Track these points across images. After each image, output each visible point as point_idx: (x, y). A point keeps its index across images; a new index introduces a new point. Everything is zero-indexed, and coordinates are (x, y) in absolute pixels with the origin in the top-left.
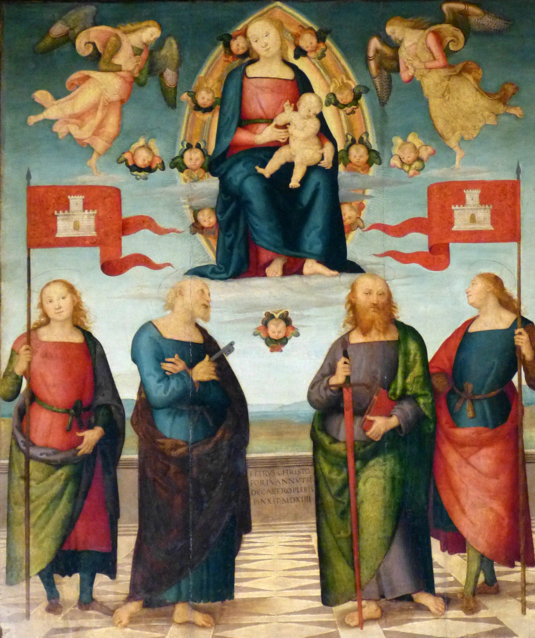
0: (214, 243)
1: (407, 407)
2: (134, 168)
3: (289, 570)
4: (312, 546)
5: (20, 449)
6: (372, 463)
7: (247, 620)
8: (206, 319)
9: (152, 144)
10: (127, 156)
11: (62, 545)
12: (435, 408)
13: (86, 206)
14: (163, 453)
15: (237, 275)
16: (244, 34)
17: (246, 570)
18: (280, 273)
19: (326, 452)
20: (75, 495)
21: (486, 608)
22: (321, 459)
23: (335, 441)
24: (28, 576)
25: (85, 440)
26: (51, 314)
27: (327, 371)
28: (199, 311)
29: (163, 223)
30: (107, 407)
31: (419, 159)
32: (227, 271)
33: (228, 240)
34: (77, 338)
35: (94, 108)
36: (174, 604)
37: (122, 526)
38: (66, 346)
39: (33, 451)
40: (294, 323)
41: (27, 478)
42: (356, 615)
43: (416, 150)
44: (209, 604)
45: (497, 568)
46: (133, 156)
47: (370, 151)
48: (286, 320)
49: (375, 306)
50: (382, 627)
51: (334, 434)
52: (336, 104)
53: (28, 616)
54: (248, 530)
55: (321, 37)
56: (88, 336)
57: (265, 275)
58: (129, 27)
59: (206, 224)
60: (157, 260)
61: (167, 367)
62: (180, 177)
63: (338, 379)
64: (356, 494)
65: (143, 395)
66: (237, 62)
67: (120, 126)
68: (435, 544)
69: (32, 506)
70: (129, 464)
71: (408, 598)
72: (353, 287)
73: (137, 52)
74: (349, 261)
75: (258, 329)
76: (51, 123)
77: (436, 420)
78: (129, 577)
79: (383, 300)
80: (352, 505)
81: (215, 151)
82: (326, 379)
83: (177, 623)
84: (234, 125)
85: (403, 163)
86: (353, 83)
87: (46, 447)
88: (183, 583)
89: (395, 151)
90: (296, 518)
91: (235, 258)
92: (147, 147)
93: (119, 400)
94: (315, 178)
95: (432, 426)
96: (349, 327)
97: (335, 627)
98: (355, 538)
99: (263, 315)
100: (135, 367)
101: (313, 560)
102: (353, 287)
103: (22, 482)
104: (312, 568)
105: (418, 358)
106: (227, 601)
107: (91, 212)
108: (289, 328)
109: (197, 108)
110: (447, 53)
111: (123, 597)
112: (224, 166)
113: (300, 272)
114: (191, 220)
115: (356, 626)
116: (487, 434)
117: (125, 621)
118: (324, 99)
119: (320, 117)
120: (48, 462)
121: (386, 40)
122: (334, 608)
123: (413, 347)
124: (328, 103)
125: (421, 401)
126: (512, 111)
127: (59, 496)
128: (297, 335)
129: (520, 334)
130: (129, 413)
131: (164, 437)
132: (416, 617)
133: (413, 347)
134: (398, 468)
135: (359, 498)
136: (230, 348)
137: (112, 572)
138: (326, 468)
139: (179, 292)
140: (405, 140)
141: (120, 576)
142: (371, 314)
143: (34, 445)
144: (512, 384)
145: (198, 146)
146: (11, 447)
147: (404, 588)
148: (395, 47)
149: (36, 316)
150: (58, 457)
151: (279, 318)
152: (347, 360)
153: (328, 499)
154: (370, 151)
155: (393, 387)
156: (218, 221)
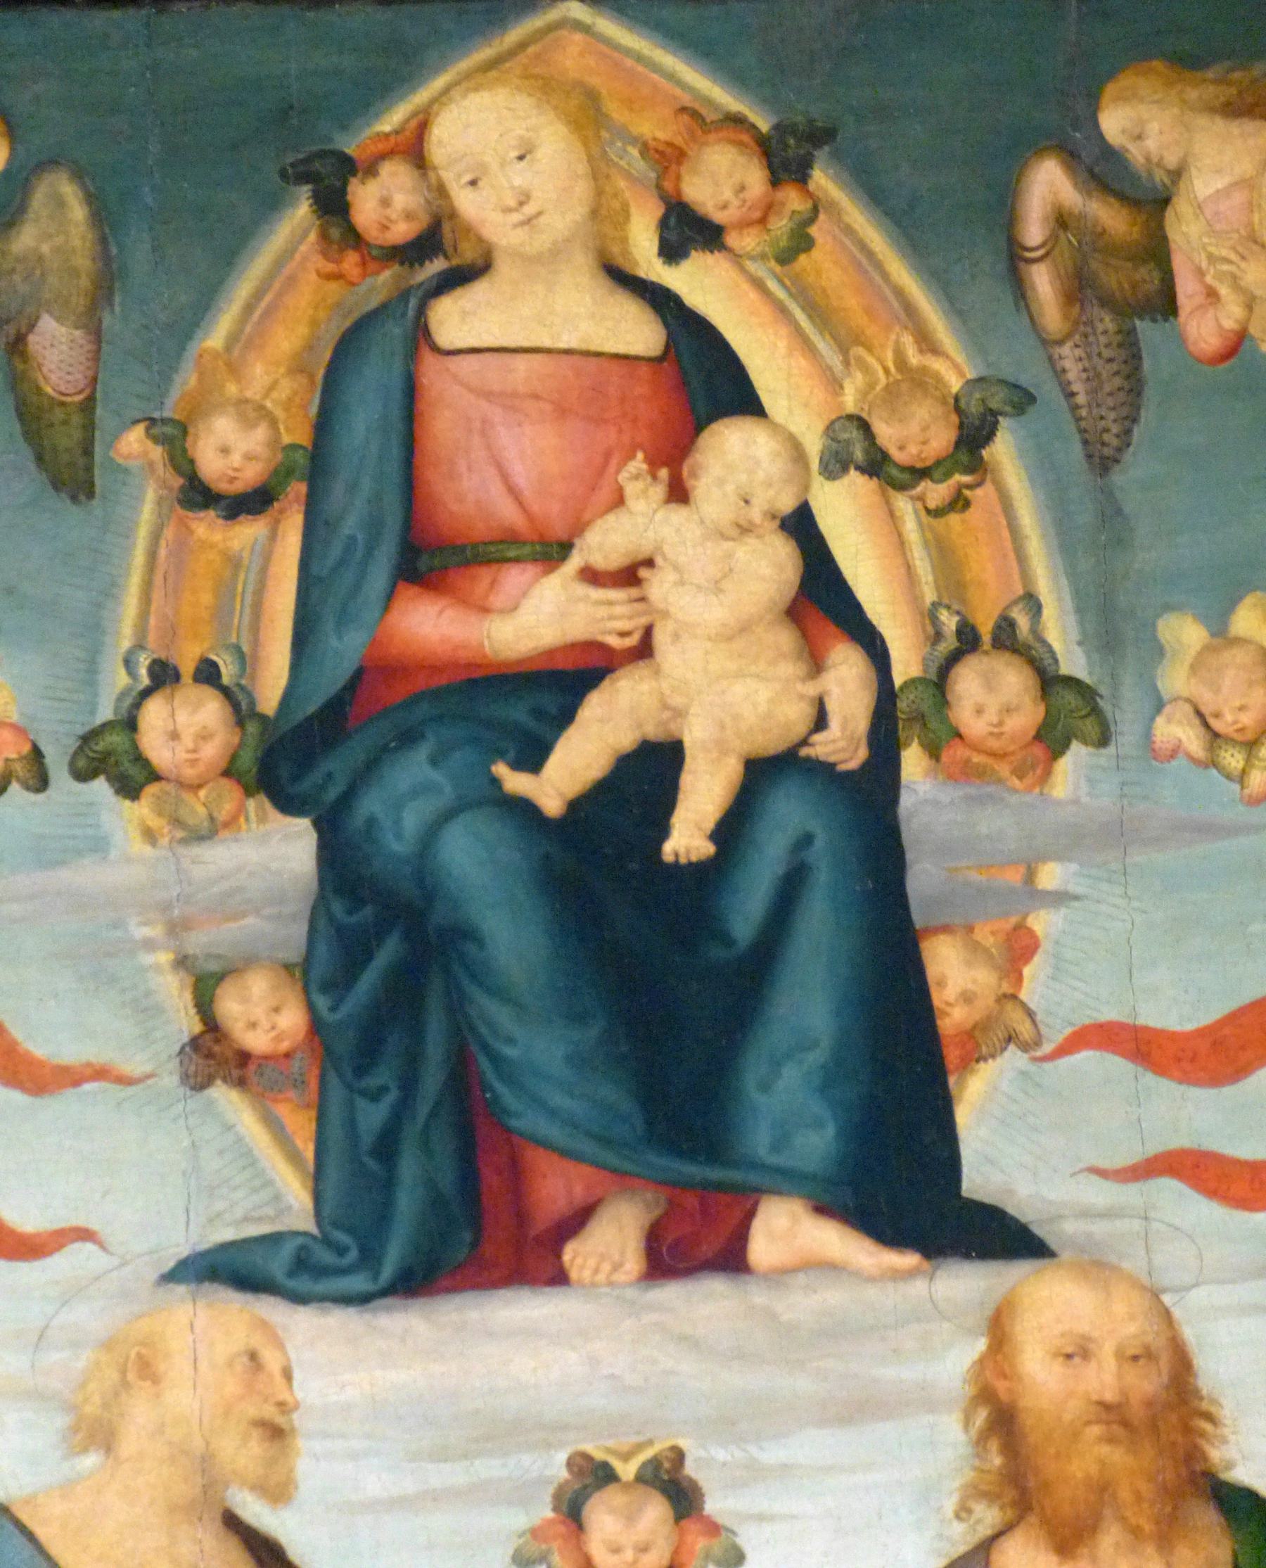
18: (634, 1263)
32: (369, 1258)
33: (373, 1116)
40: (713, 1505)
59: (257, 1042)
96: (988, 1517)
99: (556, 1468)
108: (691, 1526)
118: (814, 445)
145: (208, 674)
151: (640, 1479)
156: (316, 1026)
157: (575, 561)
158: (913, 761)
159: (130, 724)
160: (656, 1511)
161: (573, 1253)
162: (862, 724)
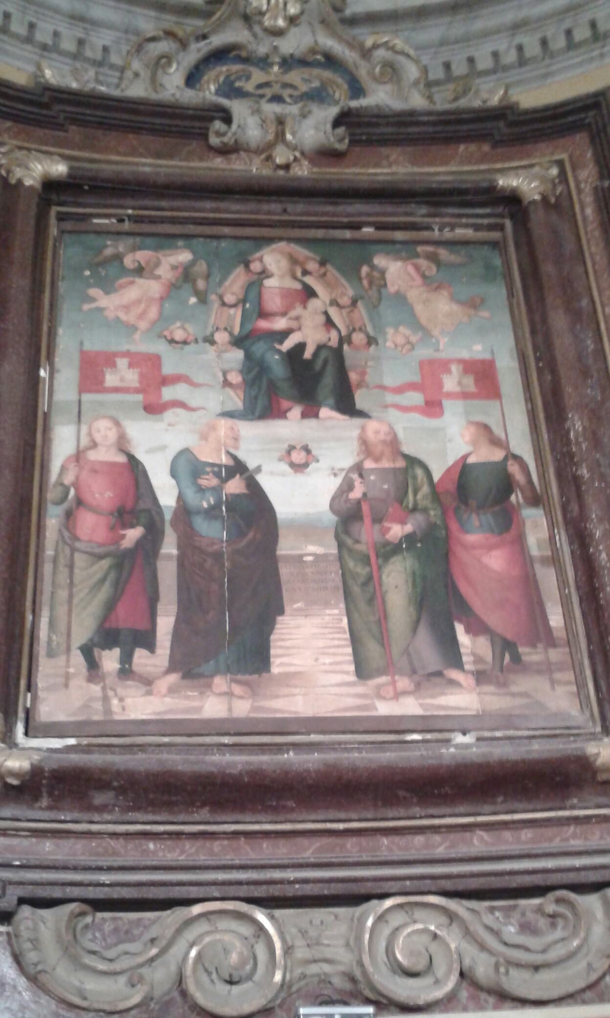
1: (419, 517)
2: (172, 341)
4: (343, 628)
5: (65, 543)
7: (286, 691)
10: (166, 333)
13: (131, 366)
16: (261, 260)
17: (281, 647)
18: (299, 416)
19: (350, 551)
20: (117, 583)
22: (346, 557)
23: (357, 542)
24: (68, 650)
25: (127, 537)
27: (346, 488)
28: (230, 442)
29: (198, 378)
30: (148, 511)
31: (409, 342)
32: (253, 413)
33: (253, 393)
34: (122, 459)
35: (138, 302)
36: (212, 676)
37: (160, 607)
39: (78, 545)
40: (314, 452)
41: (71, 567)
42: (390, 689)
43: (407, 338)
44: (247, 677)
45: (521, 650)
46: (171, 333)
48: (307, 450)
49: (384, 442)
50: (416, 699)
54: (281, 611)
55: (322, 263)
56: (132, 459)
59: (234, 382)
60: (193, 403)
61: (203, 482)
62: (211, 349)
63: (356, 494)
64: (380, 585)
65: (181, 503)
66: (256, 277)
67: (160, 314)
69: (75, 590)
70: (169, 557)
71: (439, 674)
72: (363, 429)
73: (174, 268)
74: (358, 410)
75: (282, 456)
76: (101, 310)
77: (447, 529)
78: (168, 652)
79: (389, 438)
80: (378, 594)
81: (239, 333)
82: (345, 495)
84: (255, 316)
85: (396, 346)
86: (351, 292)
89: (389, 336)
90: (327, 604)
93: (159, 506)
94: (323, 354)
95: (444, 532)
96: (362, 457)
98: (382, 620)
99: (286, 446)
102: (363, 429)
103: (66, 570)
105: (425, 479)
106: (264, 674)
108: (310, 456)
110: (424, 276)
111: (163, 669)
112: (247, 343)
113: (316, 416)
114: (221, 379)
115: (391, 699)
116: (494, 539)
118: (328, 302)
119: (326, 313)
123: (419, 472)
125: (432, 513)
127: (103, 580)
128: (318, 461)
130: (168, 516)
131: (201, 536)
133: (419, 472)
134: (417, 565)
135: (384, 588)
136: (259, 469)
137: (150, 646)
138: (351, 564)
139: (213, 428)
141: (159, 651)
145: (226, 329)
146: (57, 542)
148: (383, 272)
151: (301, 448)
152: (362, 481)
153: (356, 589)
156: (244, 380)
157: (288, 316)
158: (346, 347)
159: (213, 336)
160: (303, 454)
161: (289, 414)
162: (337, 341)
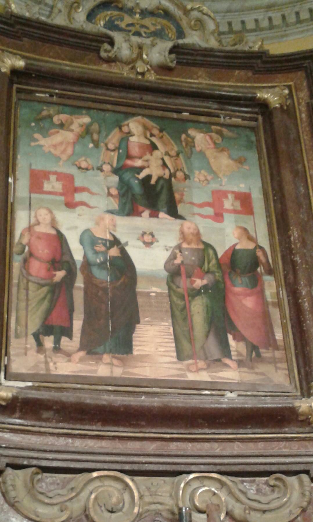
0: (117, 201)
1: (210, 276)
2: (80, 168)
3: (159, 343)
6: (197, 298)
7: (140, 364)
8: (115, 231)
9: (88, 160)
10: (77, 163)
11: (44, 323)
12: (223, 277)
13: (58, 180)
14: (96, 285)
15: (129, 215)
16: (128, 125)
18: (148, 216)
19: (174, 291)
21: (257, 368)
22: (172, 294)
23: (178, 287)
24: (26, 335)
26: (41, 220)
28: (111, 227)
29: (94, 189)
31: (206, 180)
33: (124, 201)
34: (53, 232)
35: (61, 143)
36: (102, 354)
37: (75, 315)
38: (48, 235)
39: (30, 278)
40: (156, 237)
41: (27, 289)
43: (205, 176)
47: (185, 174)
48: (152, 235)
50: (208, 372)
51: (178, 284)
52: (169, 155)
53: (26, 354)
54: (138, 322)
55: (161, 131)
56: (59, 232)
57: (141, 216)
58: (76, 116)
59: (113, 194)
60: (91, 204)
61: (97, 248)
63: (178, 261)
66: (125, 135)
67: (74, 151)
68: (230, 337)
69: (29, 303)
71: (219, 360)
73: (81, 126)
75: (139, 237)
77: (225, 283)
78: (79, 339)
79: (195, 232)
82: (172, 261)
83: (104, 363)
84: (125, 157)
85: (200, 180)
86: (176, 149)
87: (37, 277)
88: (107, 344)
89: (196, 175)
90: (162, 320)
91: (127, 208)
92: (86, 161)
94: (161, 182)
95: (223, 285)
96: (181, 241)
97: (184, 371)
99: (141, 232)
100: (81, 247)
101: (171, 339)
104: (171, 343)
107: (60, 182)
109: (108, 149)
110: (215, 143)
111: (77, 349)
113: (157, 216)
115: (195, 372)
116: (249, 291)
117: (77, 360)
118: (164, 153)
119: (163, 159)
120: (38, 284)
121: (188, 136)
122: (183, 362)
123: (211, 252)
124: (165, 155)
125: (217, 274)
126: (245, 167)
127: (44, 298)
129: (259, 251)
130: (79, 266)
132: (224, 370)
133: (211, 252)
134: (208, 301)
136: (127, 244)
137: (70, 336)
138: (175, 299)
139: (102, 219)
140: (200, 173)
141: (74, 339)
142: (191, 237)
143: (31, 275)
144: (258, 272)
145: (109, 163)
147: (217, 356)
149: (33, 221)
150: (43, 282)
154: (185, 174)
155: (203, 267)
